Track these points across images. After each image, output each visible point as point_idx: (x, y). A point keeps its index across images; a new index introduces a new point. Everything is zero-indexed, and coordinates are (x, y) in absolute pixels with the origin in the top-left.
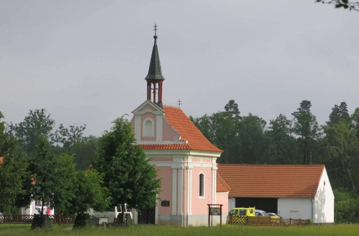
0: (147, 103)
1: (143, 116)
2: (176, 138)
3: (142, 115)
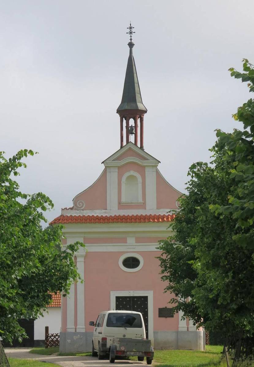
0: (128, 147)
1: (121, 169)
3: (119, 168)
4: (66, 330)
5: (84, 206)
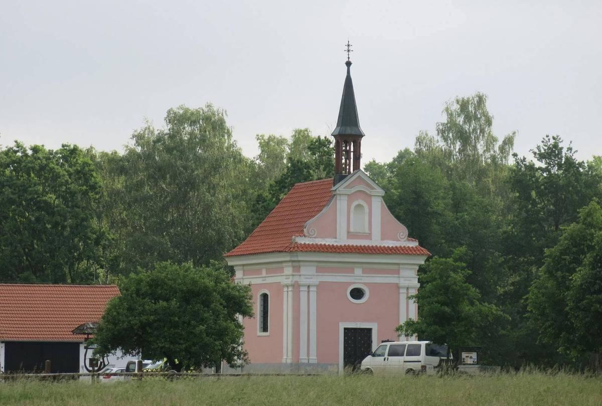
2: (402, 235)
4: (298, 361)
5: (316, 233)
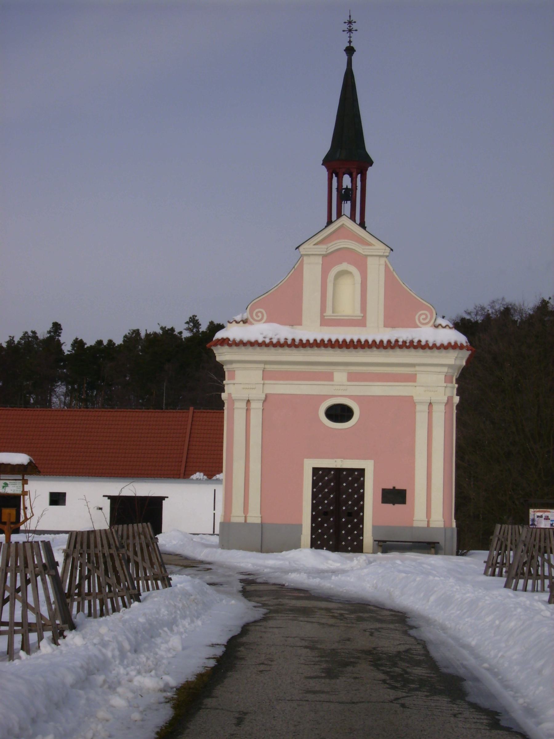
2: (424, 319)
